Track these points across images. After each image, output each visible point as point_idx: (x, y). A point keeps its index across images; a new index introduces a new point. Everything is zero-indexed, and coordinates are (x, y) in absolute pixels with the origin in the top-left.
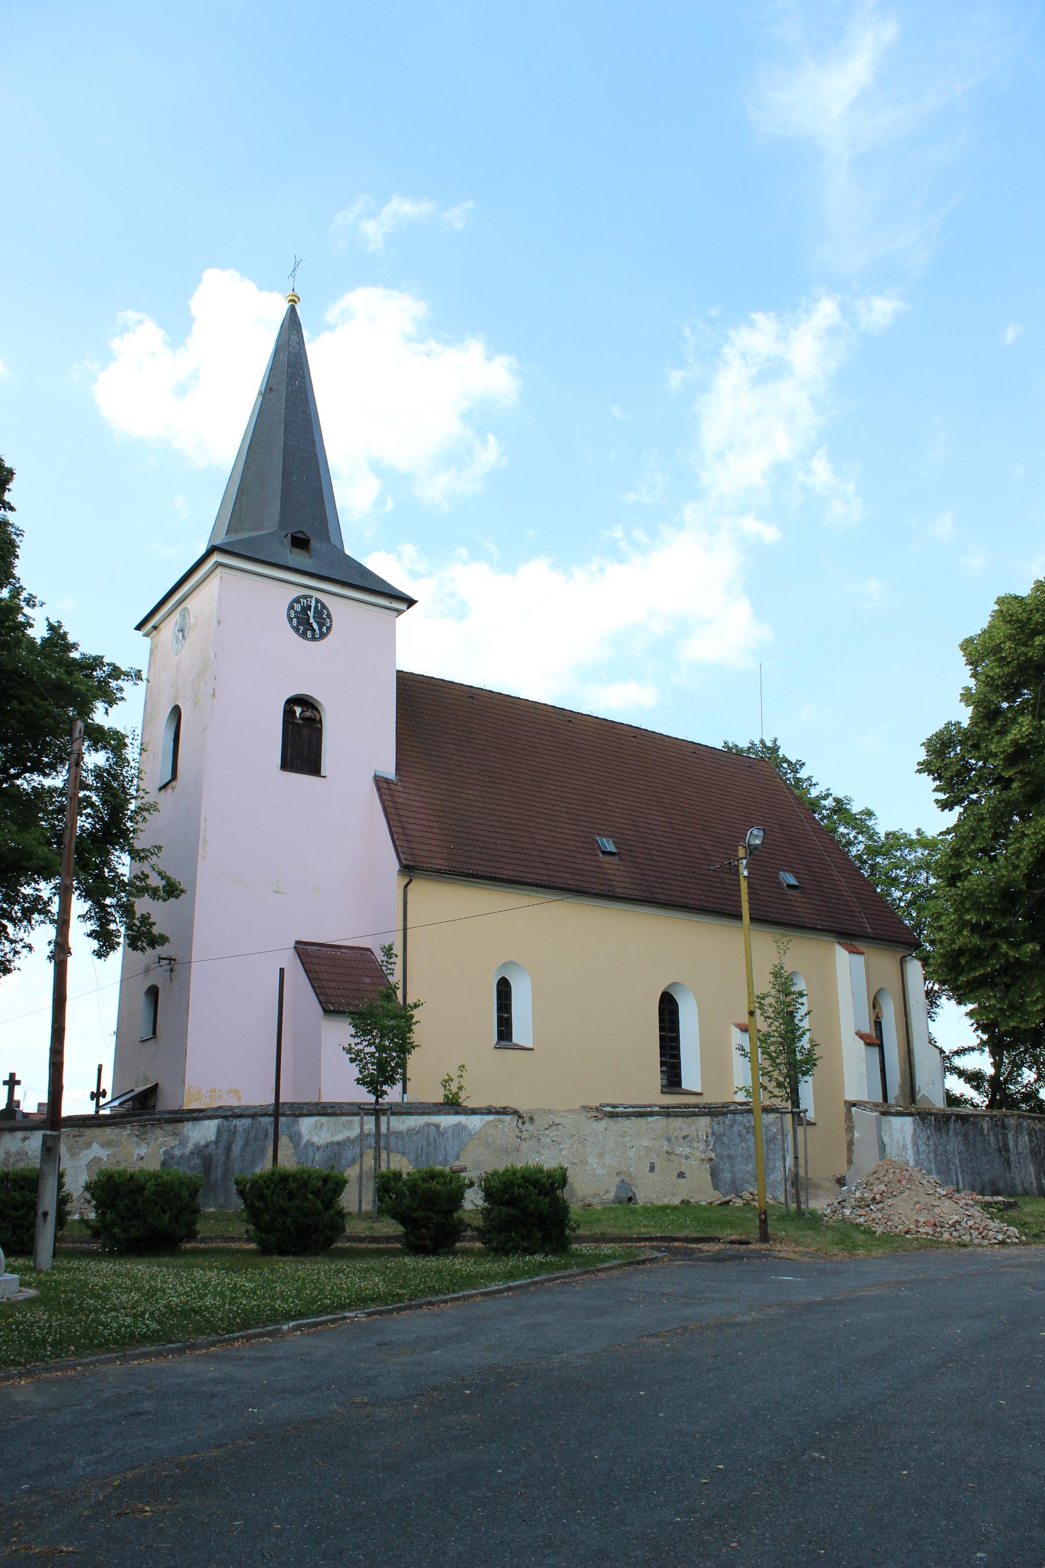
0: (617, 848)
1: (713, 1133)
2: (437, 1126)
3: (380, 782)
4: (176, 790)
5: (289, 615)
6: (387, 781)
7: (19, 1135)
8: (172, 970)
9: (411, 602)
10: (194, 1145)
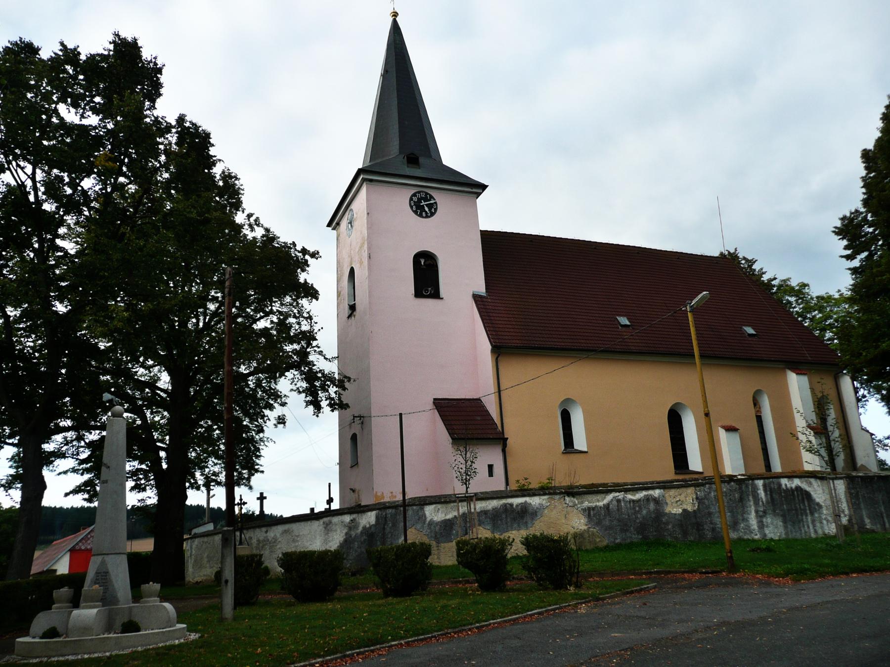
0: (630, 322)
1: (697, 498)
2: (511, 505)
3: (477, 298)
4: (356, 317)
5: (410, 204)
6: (481, 296)
7: (264, 529)
8: (362, 423)
10: (363, 528)
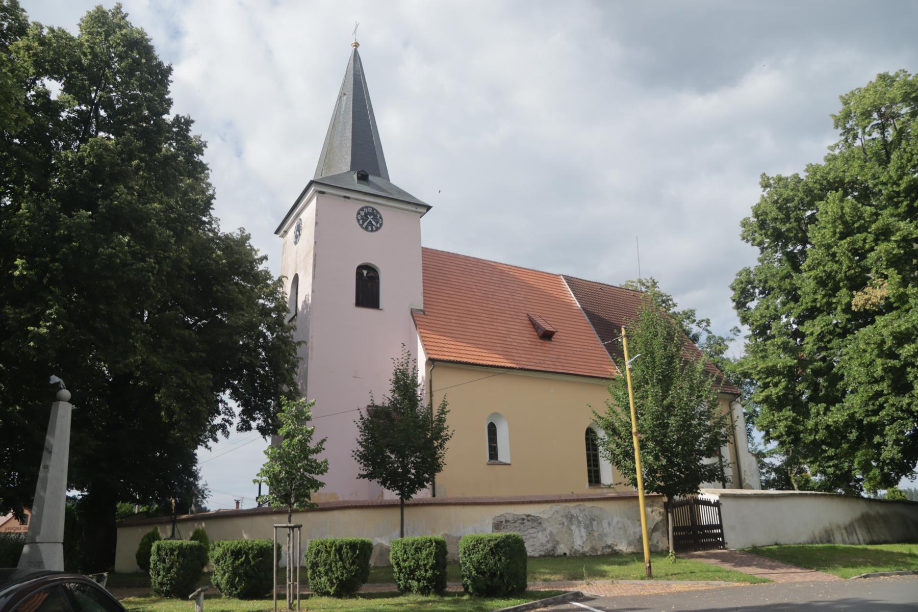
5: (357, 218)
9: (428, 208)
